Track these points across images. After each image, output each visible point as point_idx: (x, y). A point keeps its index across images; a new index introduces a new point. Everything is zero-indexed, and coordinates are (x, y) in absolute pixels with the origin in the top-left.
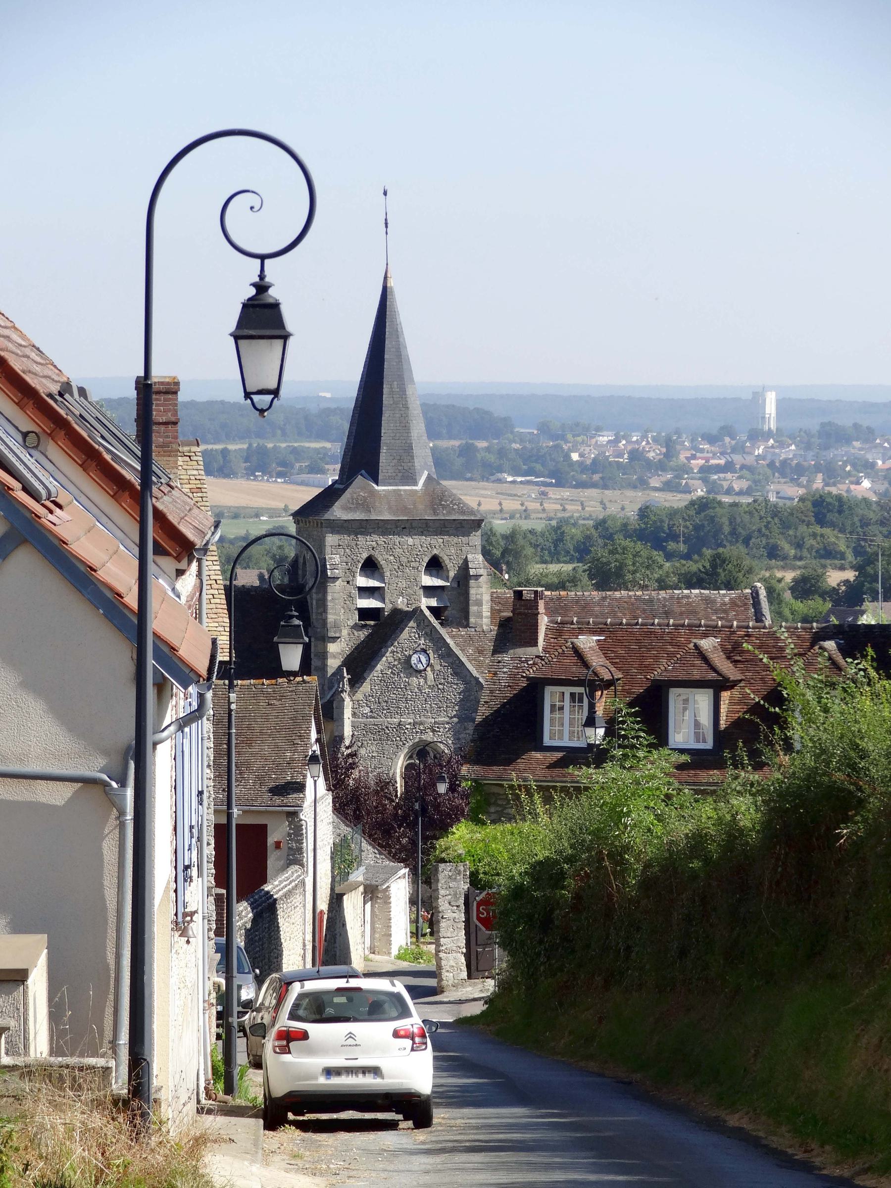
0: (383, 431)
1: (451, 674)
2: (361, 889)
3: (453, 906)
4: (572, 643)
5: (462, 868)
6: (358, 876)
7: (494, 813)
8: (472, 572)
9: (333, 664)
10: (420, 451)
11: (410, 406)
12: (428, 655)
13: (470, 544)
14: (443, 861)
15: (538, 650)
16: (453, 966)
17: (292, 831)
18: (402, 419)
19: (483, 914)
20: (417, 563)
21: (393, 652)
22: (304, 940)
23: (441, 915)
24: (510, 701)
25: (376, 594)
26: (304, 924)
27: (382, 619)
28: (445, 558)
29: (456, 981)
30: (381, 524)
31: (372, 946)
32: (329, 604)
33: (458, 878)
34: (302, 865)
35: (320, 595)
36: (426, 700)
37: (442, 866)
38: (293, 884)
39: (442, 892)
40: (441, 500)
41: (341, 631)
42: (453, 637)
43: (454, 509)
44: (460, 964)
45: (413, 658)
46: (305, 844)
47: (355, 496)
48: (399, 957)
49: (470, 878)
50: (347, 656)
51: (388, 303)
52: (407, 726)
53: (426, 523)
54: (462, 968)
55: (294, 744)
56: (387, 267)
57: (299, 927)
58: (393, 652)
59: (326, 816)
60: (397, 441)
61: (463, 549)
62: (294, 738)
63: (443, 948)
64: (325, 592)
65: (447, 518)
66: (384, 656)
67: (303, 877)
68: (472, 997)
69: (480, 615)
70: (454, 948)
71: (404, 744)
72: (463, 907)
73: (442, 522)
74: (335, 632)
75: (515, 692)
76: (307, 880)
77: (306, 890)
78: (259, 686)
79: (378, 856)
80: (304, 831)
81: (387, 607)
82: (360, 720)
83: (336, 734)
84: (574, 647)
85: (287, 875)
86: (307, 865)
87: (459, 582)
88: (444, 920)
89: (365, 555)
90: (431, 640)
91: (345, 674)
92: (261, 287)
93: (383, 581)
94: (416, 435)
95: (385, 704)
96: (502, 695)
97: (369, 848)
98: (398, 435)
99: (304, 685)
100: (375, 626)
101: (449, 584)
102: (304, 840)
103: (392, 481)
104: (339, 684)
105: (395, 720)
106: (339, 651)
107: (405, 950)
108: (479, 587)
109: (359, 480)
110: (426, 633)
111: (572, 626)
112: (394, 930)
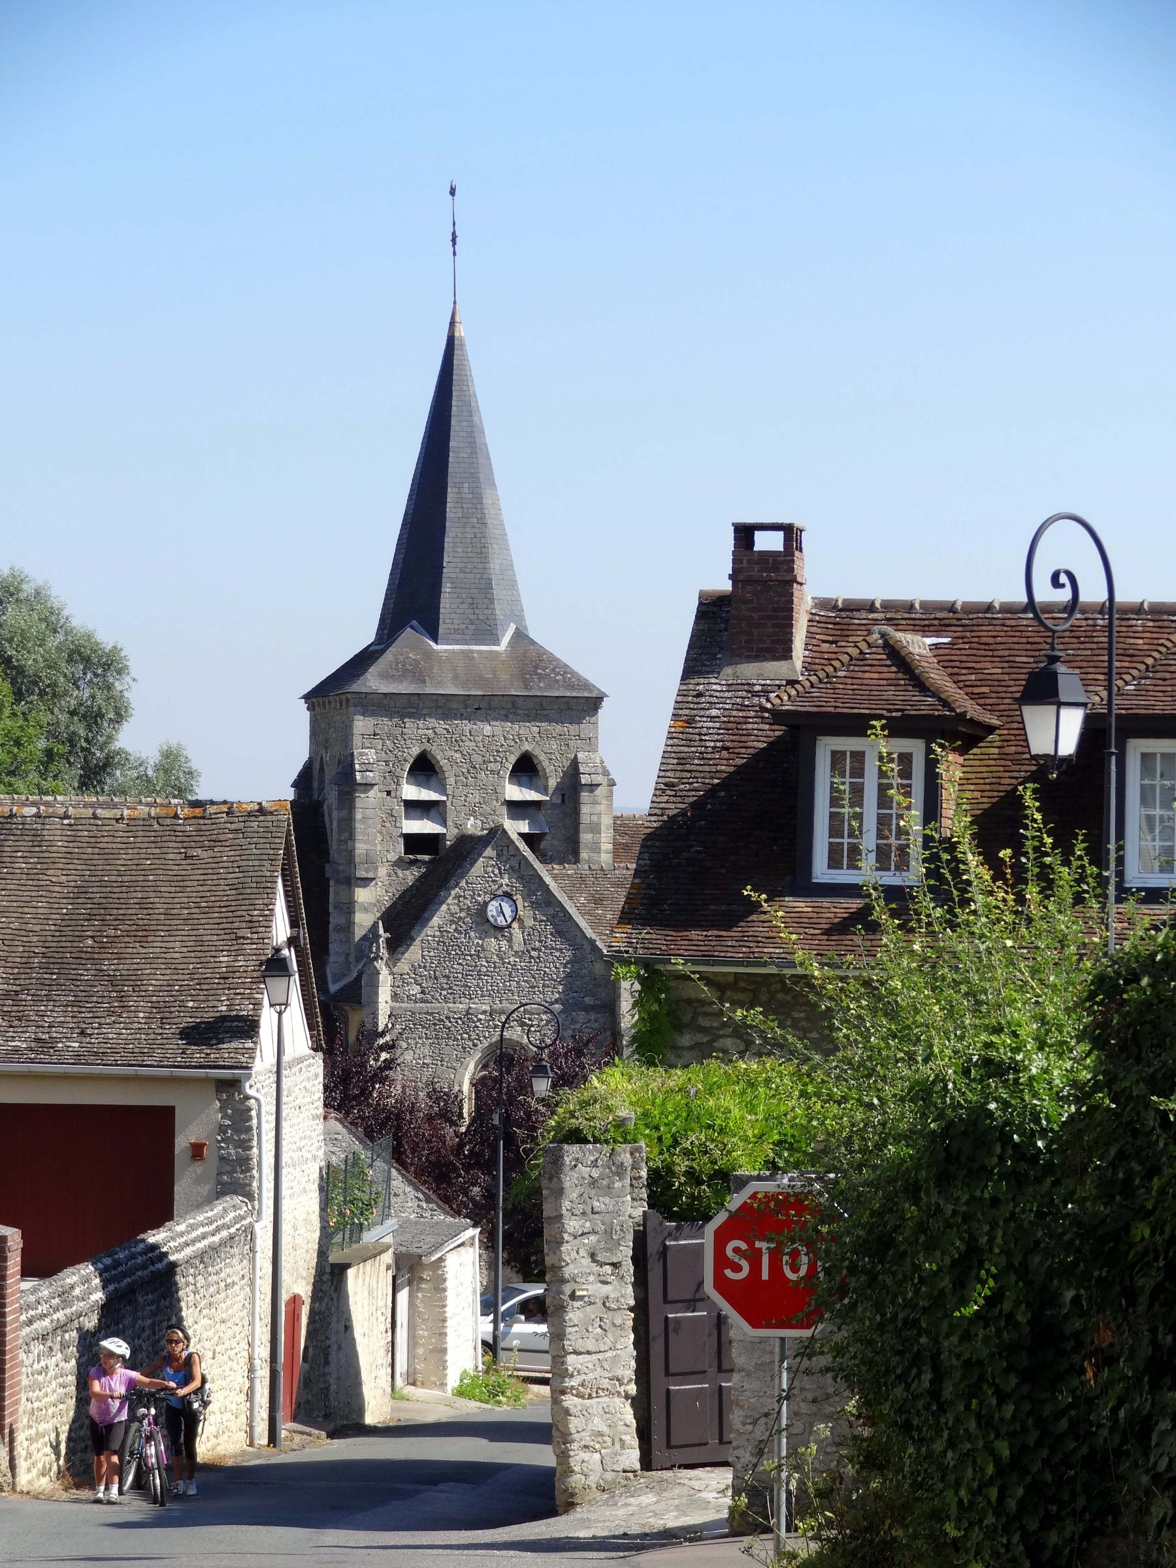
0: (446, 559)
1: (551, 934)
2: (388, 1258)
3: (601, 1264)
4: (883, 635)
5: (626, 1158)
6: (381, 1233)
7: (691, 1048)
8: (584, 780)
9: (363, 920)
10: (505, 592)
11: (489, 521)
12: (514, 902)
13: (582, 736)
14: (576, 1137)
15: (794, 669)
16: (601, 1434)
17: (228, 1122)
18: (475, 540)
19: (737, 1268)
20: (499, 765)
21: (458, 897)
22: (251, 1359)
23: (567, 1289)
24: (727, 783)
25: (433, 812)
26: (251, 1324)
27: (442, 853)
28: (542, 757)
29: (609, 1476)
30: (442, 701)
31: (411, 1370)
32: (358, 825)
33: (618, 1185)
34: (249, 1196)
35: (344, 813)
36: (510, 975)
37: (572, 1151)
38: (224, 1233)
39: (572, 1224)
40: (536, 667)
41: (376, 868)
42: (555, 877)
43: (557, 681)
44: (622, 1428)
45: (490, 907)
46: (255, 1151)
47: (401, 658)
48: (460, 1393)
49: (649, 1186)
50: (388, 909)
51: (455, 362)
52: (480, 1016)
53: (513, 703)
54: (626, 1438)
55: (237, 938)
56: (455, 307)
57: (237, 1329)
58: (458, 897)
59: (309, 1100)
60: (469, 576)
61: (571, 743)
62: (236, 925)
63: (574, 1382)
64: (352, 808)
65: (545, 694)
66: (443, 902)
67: (249, 1220)
68: (657, 1524)
69: (596, 848)
70: (605, 1383)
71: (475, 1045)
72: (628, 1268)
73: (537, 700)
74: (367, 871)
75: (739, 762)
76: (258, 1227)
77: (258, 1248)
78: (168, 821)
79: (424, 1205)
80: (255, 1122)
81: (450, 833)
82: (405, 1005)
83: (368, 1026)
84: (886, 645)
85: (210, 1214)
86: (260, 1195)
87: (563, 795)
88: (577, 1304)
89: (416, 751)
90: (521, 878)
91: (381, 931)
93: (443, 792)
94: (497, 566)
95: (444, 981)
96: (707, 768)
97: (408, 1189)
98: (469, 566)
99: (261, 818)
100: (430, 862)
101: (548, 799)
102: (255, 1143)
103: (458, 637)
104: (371, 947)
105: (461, 1006)
106: (374, 901)
107: (473, 1378)
108: (595, 803)
109: (408, 635)
110: (511, 868)
111: (871, 616)
112: (451, 1341)
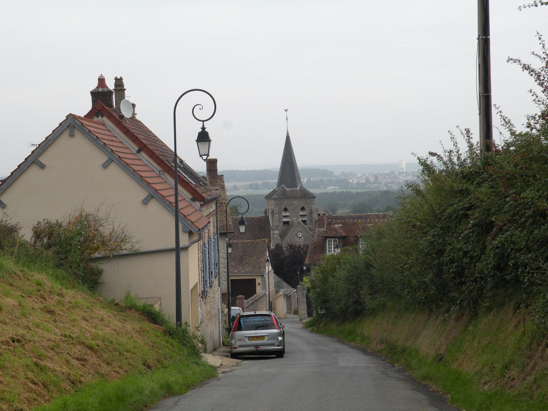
89: (284, 207)
92: (203, 128)
